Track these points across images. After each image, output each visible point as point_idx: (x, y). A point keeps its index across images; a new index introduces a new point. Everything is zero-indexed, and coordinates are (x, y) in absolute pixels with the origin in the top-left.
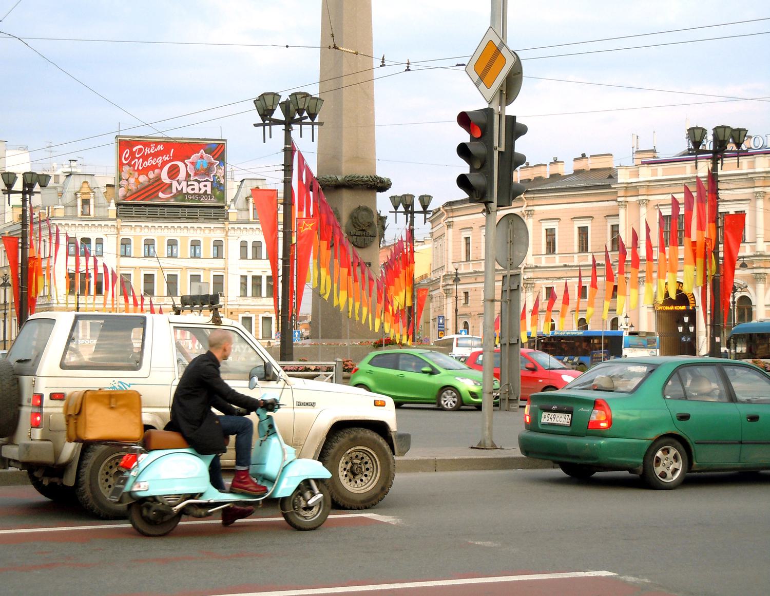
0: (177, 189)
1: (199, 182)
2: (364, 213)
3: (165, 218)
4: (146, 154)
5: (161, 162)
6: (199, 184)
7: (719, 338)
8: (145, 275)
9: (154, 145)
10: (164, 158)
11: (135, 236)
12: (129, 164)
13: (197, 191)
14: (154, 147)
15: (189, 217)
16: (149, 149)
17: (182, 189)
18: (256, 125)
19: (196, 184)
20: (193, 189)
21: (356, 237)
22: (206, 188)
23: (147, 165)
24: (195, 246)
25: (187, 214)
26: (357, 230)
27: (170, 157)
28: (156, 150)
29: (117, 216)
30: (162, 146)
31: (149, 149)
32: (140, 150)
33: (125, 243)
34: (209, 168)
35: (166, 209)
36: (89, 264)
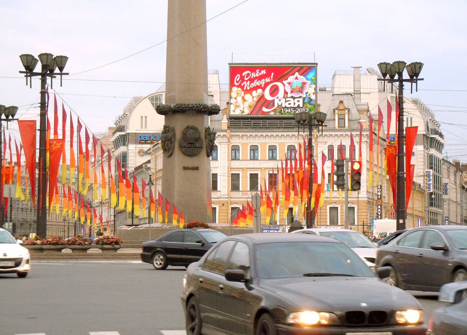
0: (278, 104)
1: (294, 98)
2: (191, 131)
3: (267, 128)
4: (252, 78)
5: (264, 83)
6: (294, 100)
7: (402, 220)
8: (250, 174)
9: (259, 70)
10: (266, 80)
11: (242, 144)
12: (239, 86)
13: (292, 105)
14: (258, 72)
15: (286, 126)
16: (255, 73)
17: (282, 104)
18: (20, 72)
19: (292, 100)
20: (290, 104)
21: (185, 148)
22: (298, 103)
23: (253, 86)
24: (235, 150)
25: (284, 124)
26: (188, 143)
27: (271, 79)
28: (260, 74)
29: (228, 127)
30: (265, 70)
31: (255, 73)
32: (248, 75)
33: (235, 149)
34: (303, 87)
35: (267, 121)
36: (420, 159)
